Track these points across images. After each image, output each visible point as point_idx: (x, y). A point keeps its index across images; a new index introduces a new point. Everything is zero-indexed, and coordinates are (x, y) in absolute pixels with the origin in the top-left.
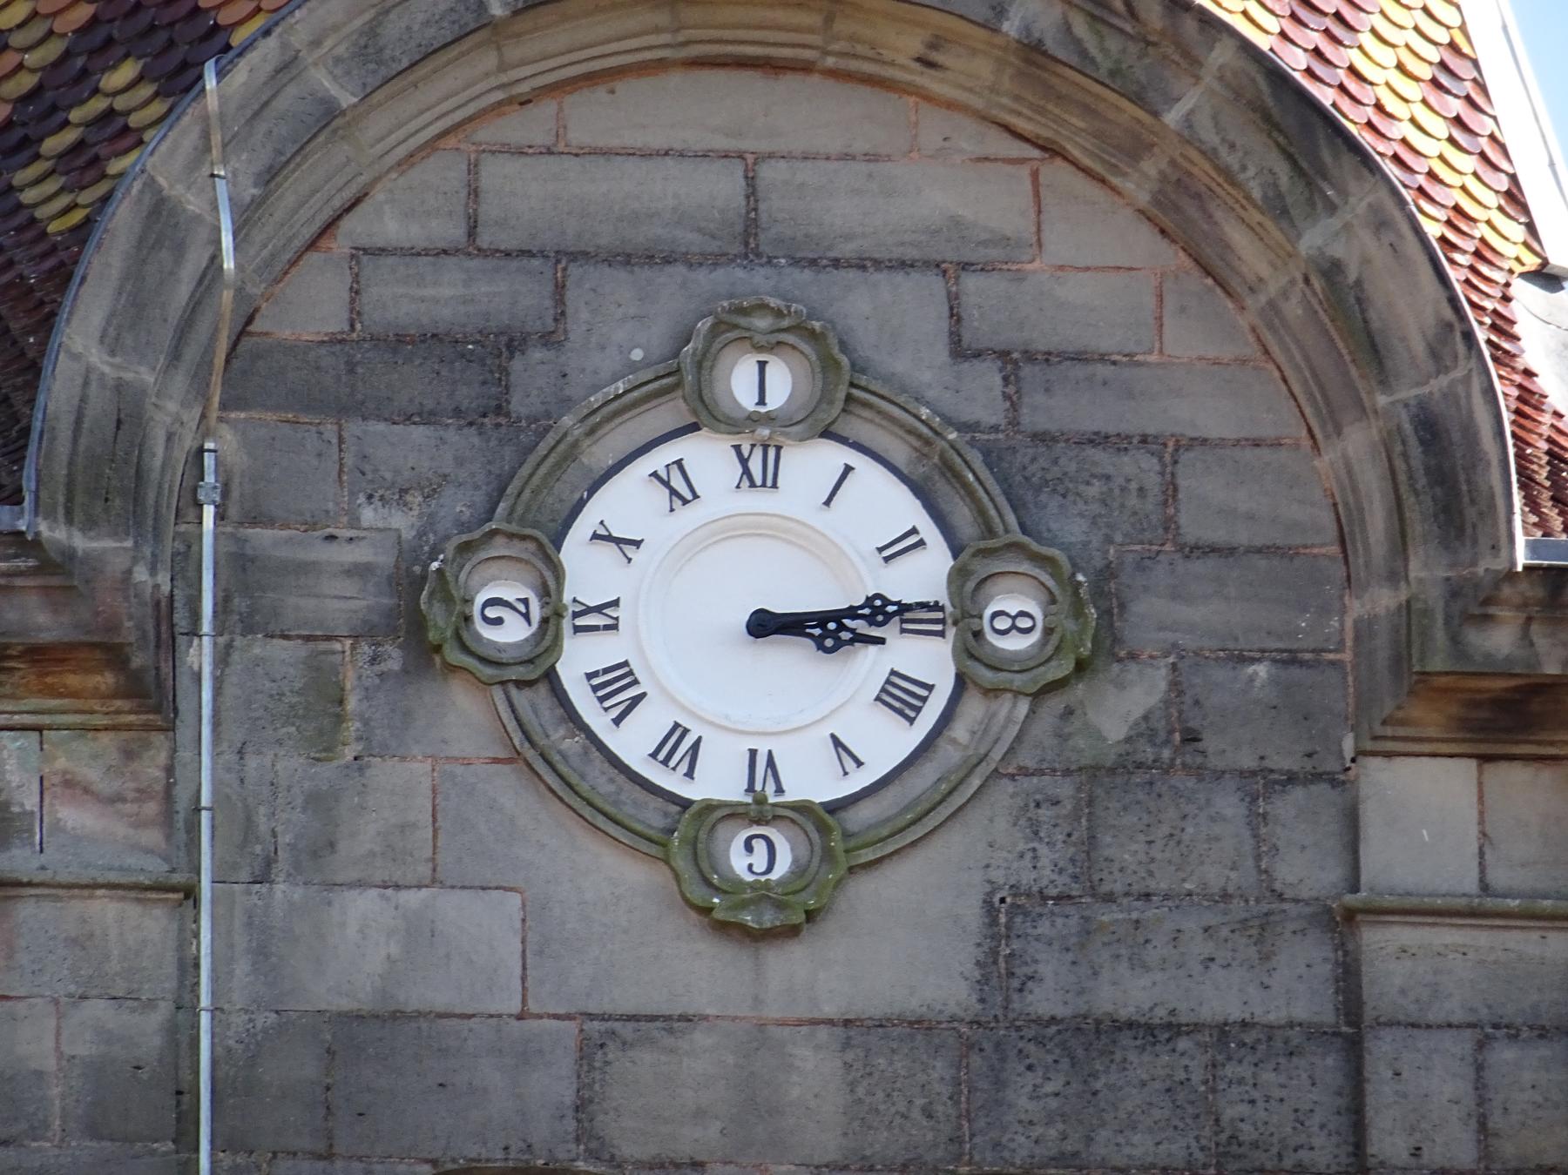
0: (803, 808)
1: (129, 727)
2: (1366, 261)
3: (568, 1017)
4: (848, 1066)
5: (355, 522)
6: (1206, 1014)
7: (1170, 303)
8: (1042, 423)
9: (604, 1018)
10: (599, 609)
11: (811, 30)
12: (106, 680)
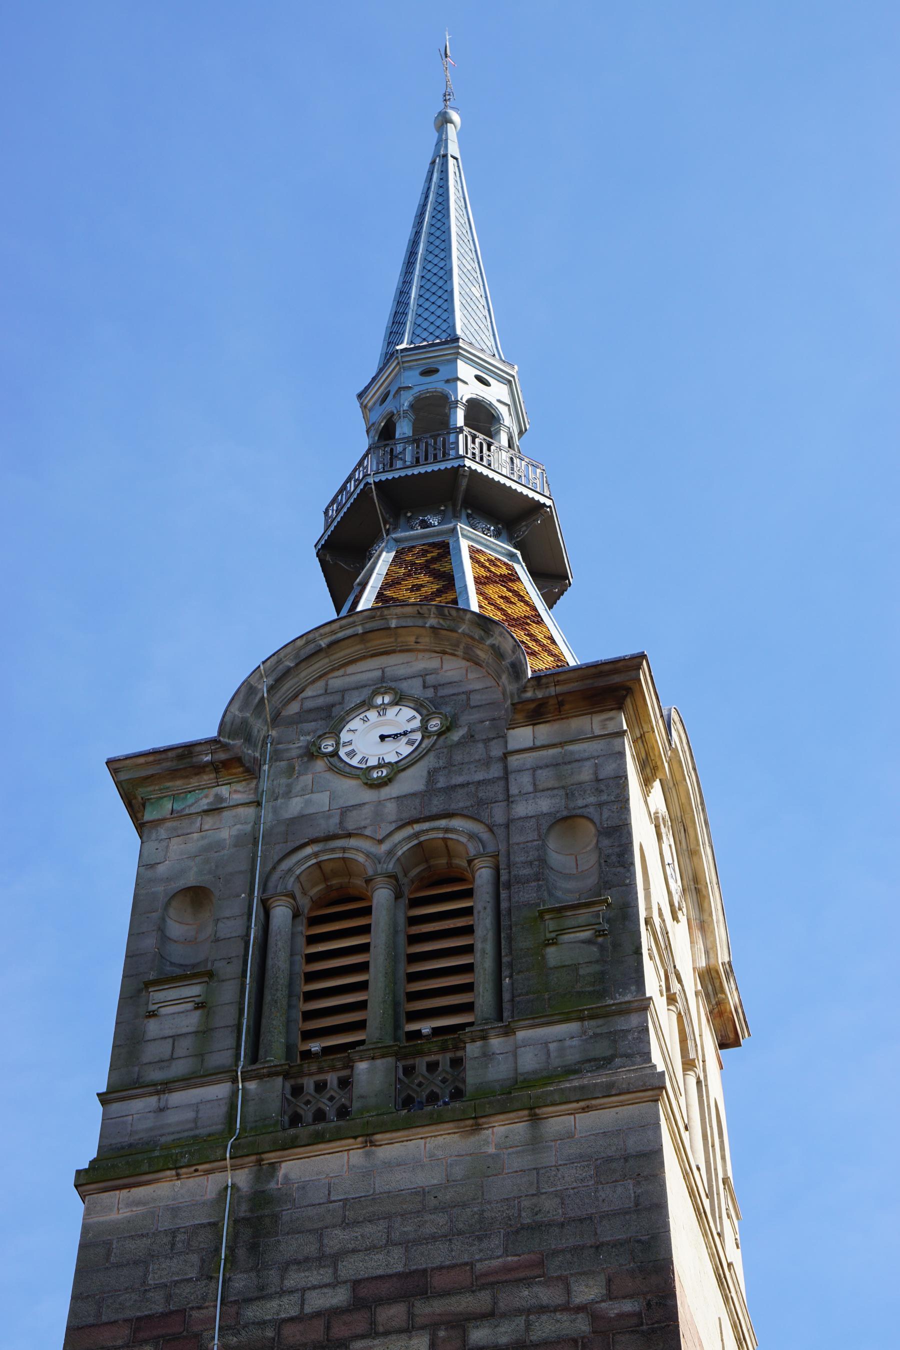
0: (389, 763)
1: (248, 779)
2: (500, 642)
3: (339, 809)
4: (398, 804)
5: (299, 740)
6: (475, 780)
7: (469, 671)
8: (441, 695)
9: (346, 807)
10: (348, 742)
11: (392, 642)
12: (241, 769)
